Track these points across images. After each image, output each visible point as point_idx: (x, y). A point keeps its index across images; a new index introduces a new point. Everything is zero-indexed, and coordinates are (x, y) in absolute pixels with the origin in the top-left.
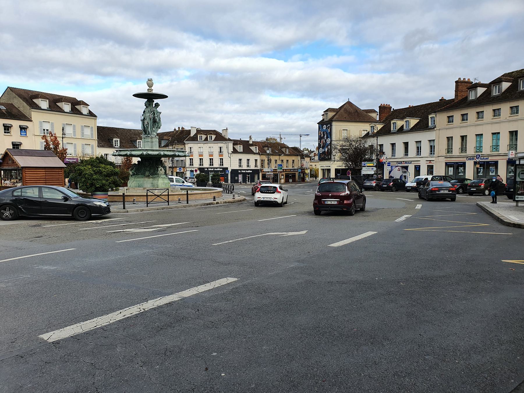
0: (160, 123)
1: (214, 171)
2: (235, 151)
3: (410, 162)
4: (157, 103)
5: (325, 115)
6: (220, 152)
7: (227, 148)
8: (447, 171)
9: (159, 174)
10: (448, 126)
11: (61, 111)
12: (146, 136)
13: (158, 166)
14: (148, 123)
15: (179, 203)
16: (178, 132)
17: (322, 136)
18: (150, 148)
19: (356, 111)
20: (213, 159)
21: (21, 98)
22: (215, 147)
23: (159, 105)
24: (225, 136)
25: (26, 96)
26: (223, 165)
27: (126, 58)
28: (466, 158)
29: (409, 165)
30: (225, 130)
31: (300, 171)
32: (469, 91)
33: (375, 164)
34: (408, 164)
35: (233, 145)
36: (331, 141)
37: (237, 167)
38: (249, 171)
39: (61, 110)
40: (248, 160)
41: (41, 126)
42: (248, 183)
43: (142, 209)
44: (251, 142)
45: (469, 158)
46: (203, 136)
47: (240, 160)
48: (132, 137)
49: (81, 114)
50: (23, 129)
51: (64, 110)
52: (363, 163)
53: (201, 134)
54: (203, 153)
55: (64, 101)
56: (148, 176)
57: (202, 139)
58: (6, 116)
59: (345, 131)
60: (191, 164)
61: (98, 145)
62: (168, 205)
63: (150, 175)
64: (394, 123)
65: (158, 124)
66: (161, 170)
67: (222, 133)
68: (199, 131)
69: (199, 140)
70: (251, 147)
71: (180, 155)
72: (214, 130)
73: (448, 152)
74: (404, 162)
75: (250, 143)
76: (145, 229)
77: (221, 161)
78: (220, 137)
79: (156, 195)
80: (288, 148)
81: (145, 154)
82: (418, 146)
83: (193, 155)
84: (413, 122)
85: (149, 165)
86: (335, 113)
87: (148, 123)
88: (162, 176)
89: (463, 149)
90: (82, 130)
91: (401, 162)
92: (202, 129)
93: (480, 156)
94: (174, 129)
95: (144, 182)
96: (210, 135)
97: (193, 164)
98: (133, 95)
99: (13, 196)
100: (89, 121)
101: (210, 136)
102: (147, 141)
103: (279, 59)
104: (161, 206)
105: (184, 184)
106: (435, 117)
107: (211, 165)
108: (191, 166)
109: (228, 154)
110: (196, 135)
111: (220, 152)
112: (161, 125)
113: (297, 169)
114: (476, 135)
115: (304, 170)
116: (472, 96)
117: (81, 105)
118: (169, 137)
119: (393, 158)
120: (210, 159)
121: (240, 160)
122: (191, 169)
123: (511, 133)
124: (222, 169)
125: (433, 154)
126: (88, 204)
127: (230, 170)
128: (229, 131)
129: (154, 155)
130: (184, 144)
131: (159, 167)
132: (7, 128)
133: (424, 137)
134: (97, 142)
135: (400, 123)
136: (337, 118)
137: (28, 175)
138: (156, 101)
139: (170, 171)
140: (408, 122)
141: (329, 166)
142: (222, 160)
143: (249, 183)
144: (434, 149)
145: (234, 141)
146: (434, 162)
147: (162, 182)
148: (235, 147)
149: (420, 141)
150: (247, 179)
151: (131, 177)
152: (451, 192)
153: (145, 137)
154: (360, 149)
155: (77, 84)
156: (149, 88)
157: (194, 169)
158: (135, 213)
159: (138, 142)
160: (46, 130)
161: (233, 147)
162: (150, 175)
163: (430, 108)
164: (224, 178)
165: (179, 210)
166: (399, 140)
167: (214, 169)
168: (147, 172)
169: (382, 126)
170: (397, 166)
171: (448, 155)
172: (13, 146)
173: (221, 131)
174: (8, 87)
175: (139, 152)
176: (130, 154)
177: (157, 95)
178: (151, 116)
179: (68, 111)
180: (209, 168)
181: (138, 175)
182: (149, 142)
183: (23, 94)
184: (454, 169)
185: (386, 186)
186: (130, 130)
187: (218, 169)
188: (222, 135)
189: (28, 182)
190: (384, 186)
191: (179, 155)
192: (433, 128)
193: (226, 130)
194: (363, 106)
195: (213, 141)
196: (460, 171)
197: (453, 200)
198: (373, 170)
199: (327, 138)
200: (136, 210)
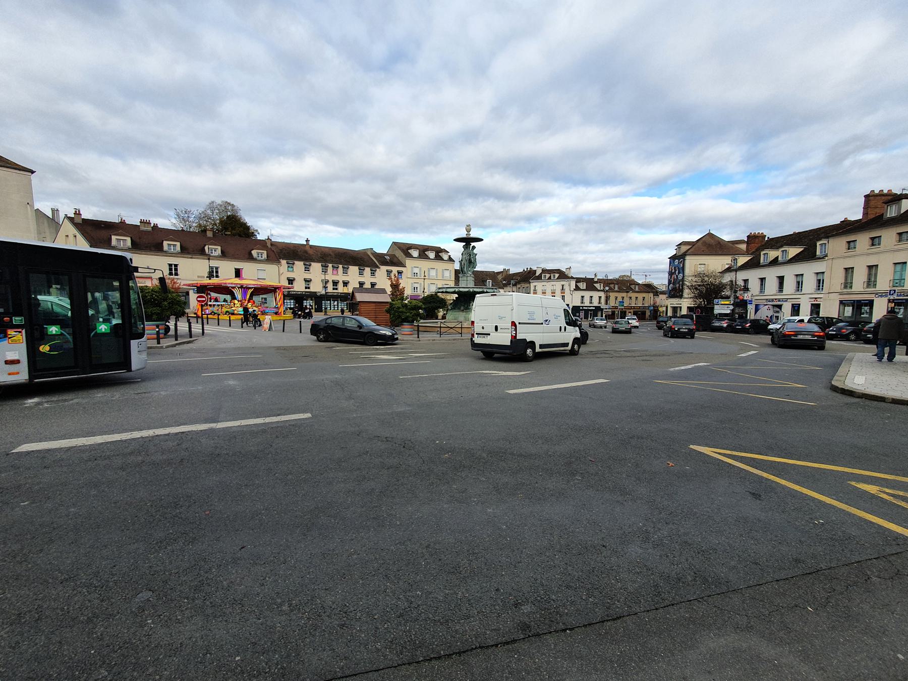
2: (577, 288)
3: (786, 300)
5: (678, 249)
6: (563, 289)
10: (847, 254)
17: (673, 271)
19: (719, 243)
28: (874, 294)
29: (784, 303)
31: (652, 308)
32: (886, 206)
33: (732, 302)
34: (782, 303)
36: (683, 276)
37: (578, 304)
39: (427, 258)
44: (596, 280)
45: (880, 294)
46: (546, 274)
51: (412, 256)
52: (716, 301)
59: (703, 266)
64: (764, 254)
69: (543, 278)
70: (595, 285)
73: (845, 287)
74: (777, 300)
79: (449, 327)
80: (638, 284)
82: (798, 280)
84: (793, 251)
86: (690, 247)
89: (871, 281)
91: (772, 300)
93: (896, 291)
99: (326, 323)
100: (449, 266)
103: (651, 196)
106: (827, 243)
111: (563, 289)
113: (649, 307)
114: (895, 264)
115: (657, 307)
119: (797, 293)
125: (821, 290)
126: (376, 333)
128: (572, 270)
129: (465, 292)
130: (530, 283)
133: (808, 270)
135: (772, 254)
136: (692, 252)
137: (363, 308)
138: (473, 244)
140: (786, 252)
141: (681, 304)
144: (823, 283)
145: (577, 278)
146: (822, 300)
148: (577, 284)
149: (802, 275)
152: (816, 338)
154: (714, 285)
161: (576, 284)
163: (823, 233)
166: (771, 275)
169: (750, 258)
170: (766, 305)
171: (845, 290)
183: (402, 246)
184: (853, 309)
185: (740, 327)
186: (483, 272)
190: (737, 327)
192: (822, 258)
194: (726, 236)
196: (863, 311)
197: (821, 347)
198: (729, 309)
199: (679, 273)
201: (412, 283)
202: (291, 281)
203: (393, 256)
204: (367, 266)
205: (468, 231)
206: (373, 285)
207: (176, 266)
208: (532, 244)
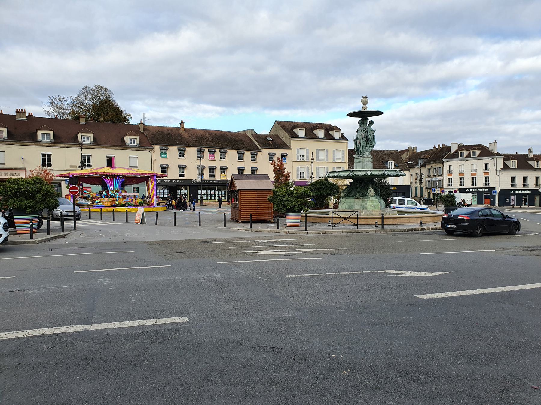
0: (374, 141)
1: (477, 191)
2: (506, 168)
4: (371, 120)
6: (486, 169)
7: (495, 164)
9: (368, 196)
12: (359, 156)
13: (368, 188)
14: (360, 142)
15: (376, 228)
16: (438, 150)
18: (361, 169)
20: (464, 178)
21: (284, 129)
22: (479, 164)
23: (374, 123)
24: (492, 150)
26: (488, 185)
27: (410, 77)
30: (493, 143)
35: (504, 160)
37: (508, 187)
38: (526, 192)
39: (315, 137)
40: (525, 178)
41: (298, 153)
42: (525, 206)
43: (324, 232)
44: (531, 156)
46: (464, 151)
47: (513, 178)
48: (384, 158)
49: (334, 139)
51: (318, 137)
53: (463, 150)
54: (464, 172)
55: (318, 129)
56: (359, 198)
57: (463, 156)
58: (271, 146)
60: (450, 184)
61: (348, 168)
62: (358, 229)
63: (361, 196)
65: (371, 143)
66: (371, 191)
67: (488, 147)
68: (461, 147)
71: (391, 174)
72: (479, 144)
75: (530, 157)
76: (278, 251)
77: (487, 180)
79: (342, 218)
81: (351, 175)
83: (476, 173)
85: (360, 187)
87: (360, 142)
88: (371, 198)
90: (334, 154)
92: (465, 145)
94: (434, 146)
95: (354, 204)
96: (473, 151)
97: (452, 184)
98: (347, 115)
101: (473, 152)
102: (359, 161)
104: (351, 229)
105: (417, 207)
107: (473, 185)
108: (449, 187)
109: (496, 171)
110: (457, 152)
112: (375, 144)
117: (333, 130)
118: (428, 156)
120: (473, 178)
121: (513, 178)
122: (450, 189)
124: (487, 190)
127: (498, 190)
128: (498, 145)
129: (361, 176)
130: (443, 162)
131: (369, 188)
134: (348, 165)
138: (370, 119)
139: (427, 192)
142: (487, 179)
143: (526, 206)
147: (371, 204)
150: (523, 202)
151: (342, 199)
153: (357, 158)
156: (363, 105)
157: (453, 190)
158: (314, 235)
159: (390, 162)
160: (302, 156)
162: (360, 197)
164: (490, 200)
165: (368, 235)
167: (477, 190)
168: (357, 194)
172: (209, 170)
173: (487, 145)
174: (276, 121)
175: (347, 173)
176: (337, 176)
177: (370, 112)
178: (364, 135)
179: (322, 137)
180: (471, 188)
181: (350, 196)
182: (361, 162)
183: (287, 126)
186: (383, 151)
187: (483, 190)
188: (489, 149)
189: (242, 202)
191: (389, 174)
193: (494, 143)
195: (477, 157)
200: (318, 232)
204: (189, 146)
205: (365, 103)
206: (254, 170)
207: (49, 156)
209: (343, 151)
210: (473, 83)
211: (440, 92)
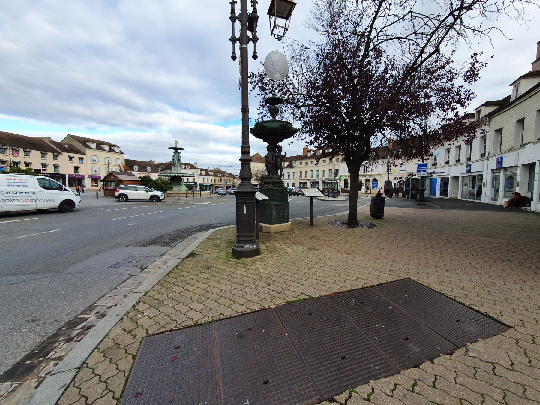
2: (201, 174)
8: (300, 185)
11: (103, 150)
25: (81, 140)
35: (200, 171)
37: (202, 183)
44: (209, 170)
50: (80, 159)
78: (193, 167)
89: (306, 176)
90: (116, 161)
116: (309, 155)
123: (323, 170)
127: (198, 184)
132: (71, 158)
138: (179, 151)
155: (91, 129)
201: (92, 167)
202: (44, 166)
203: (71, 146)
204: (49, 152)
206: (27, 164)
208: (149, 142)
209: (122, 160)
210: (165, 128)
211: (147, 129)
